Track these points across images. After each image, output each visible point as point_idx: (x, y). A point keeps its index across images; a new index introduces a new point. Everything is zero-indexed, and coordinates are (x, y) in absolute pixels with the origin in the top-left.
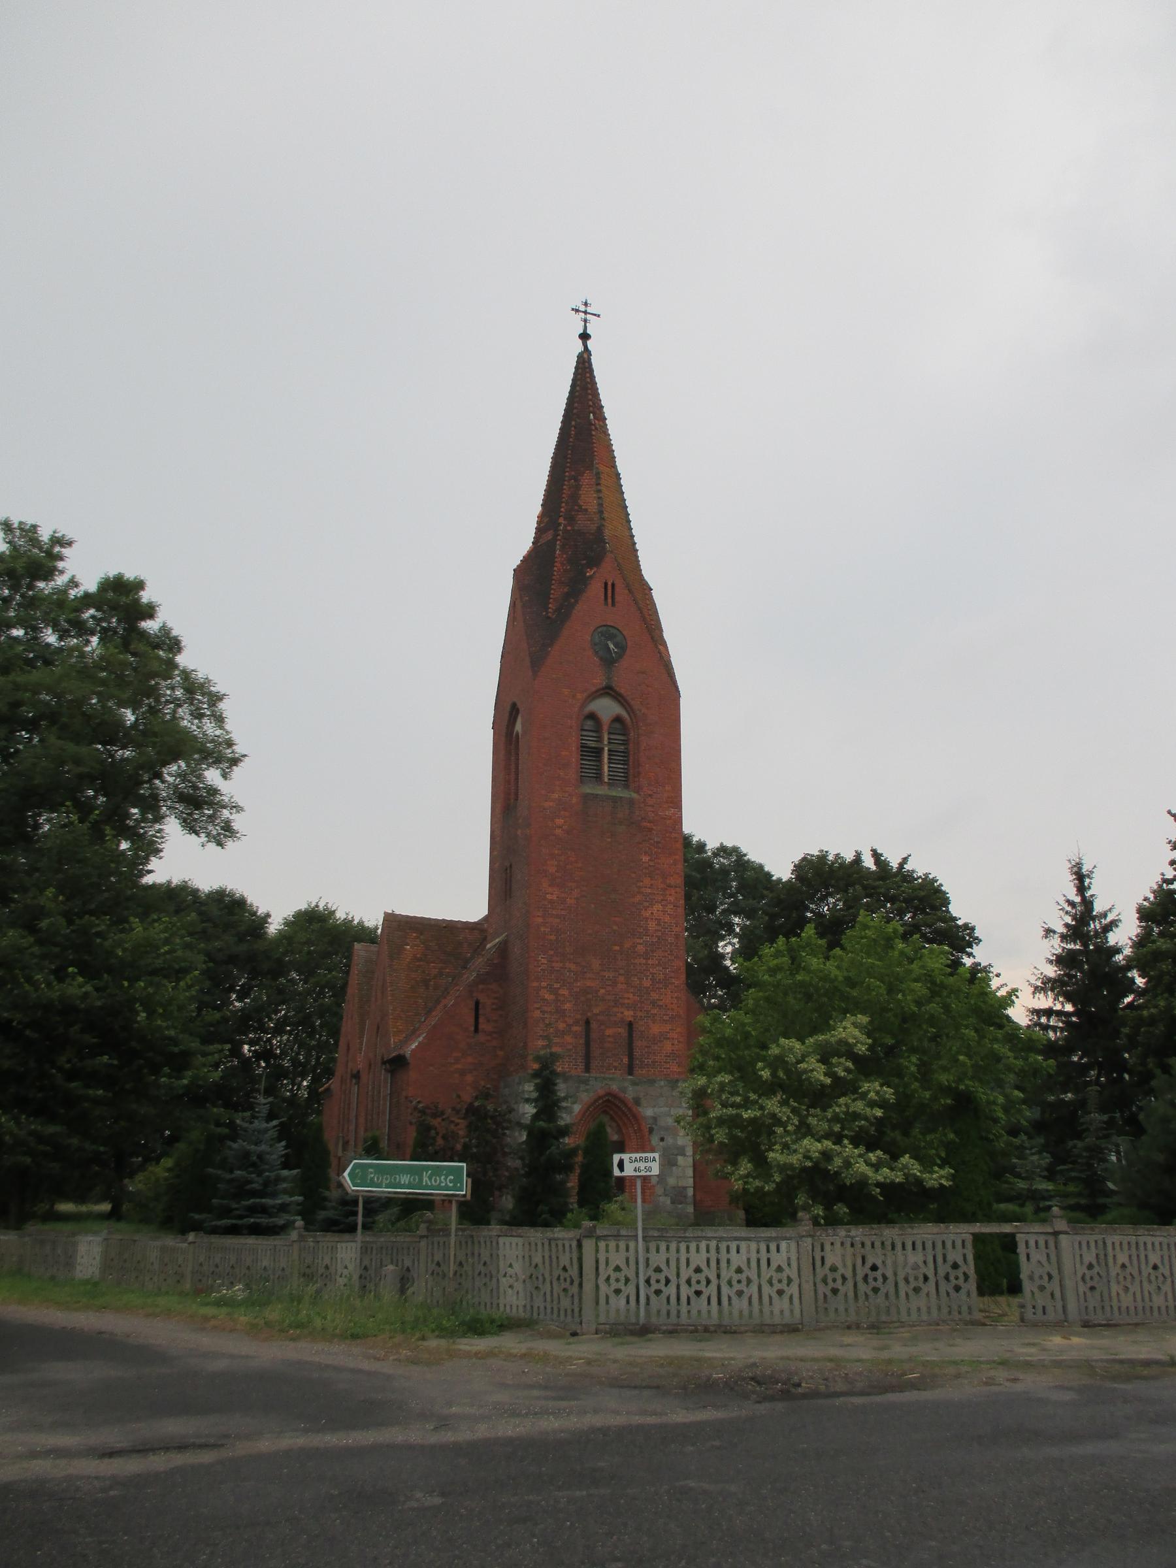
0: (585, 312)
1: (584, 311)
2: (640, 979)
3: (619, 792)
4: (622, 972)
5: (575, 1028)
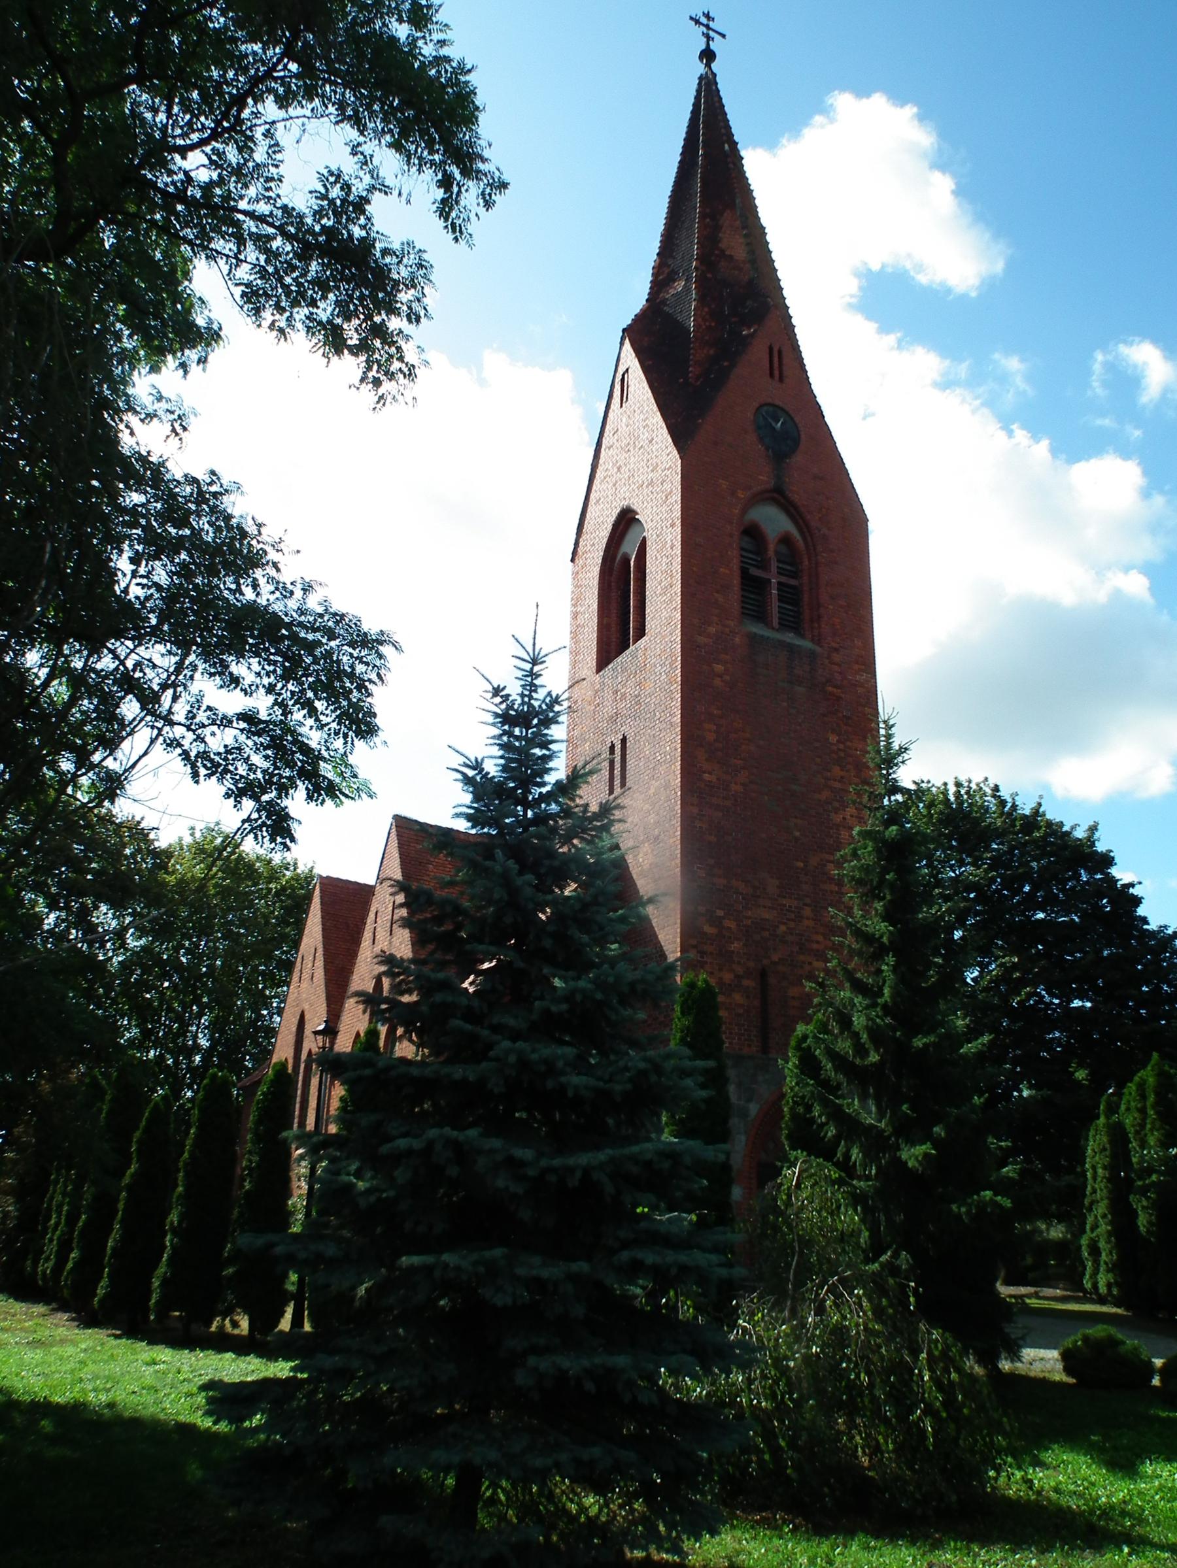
0: (708, 27)
1: (704, 21)
2: (1012, 915)
3: (789, 637)
4: (808, 901)
5: (746, 982)
